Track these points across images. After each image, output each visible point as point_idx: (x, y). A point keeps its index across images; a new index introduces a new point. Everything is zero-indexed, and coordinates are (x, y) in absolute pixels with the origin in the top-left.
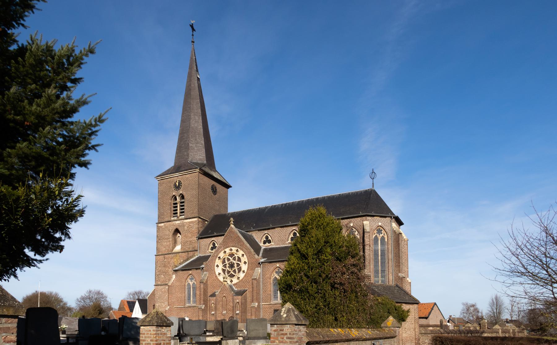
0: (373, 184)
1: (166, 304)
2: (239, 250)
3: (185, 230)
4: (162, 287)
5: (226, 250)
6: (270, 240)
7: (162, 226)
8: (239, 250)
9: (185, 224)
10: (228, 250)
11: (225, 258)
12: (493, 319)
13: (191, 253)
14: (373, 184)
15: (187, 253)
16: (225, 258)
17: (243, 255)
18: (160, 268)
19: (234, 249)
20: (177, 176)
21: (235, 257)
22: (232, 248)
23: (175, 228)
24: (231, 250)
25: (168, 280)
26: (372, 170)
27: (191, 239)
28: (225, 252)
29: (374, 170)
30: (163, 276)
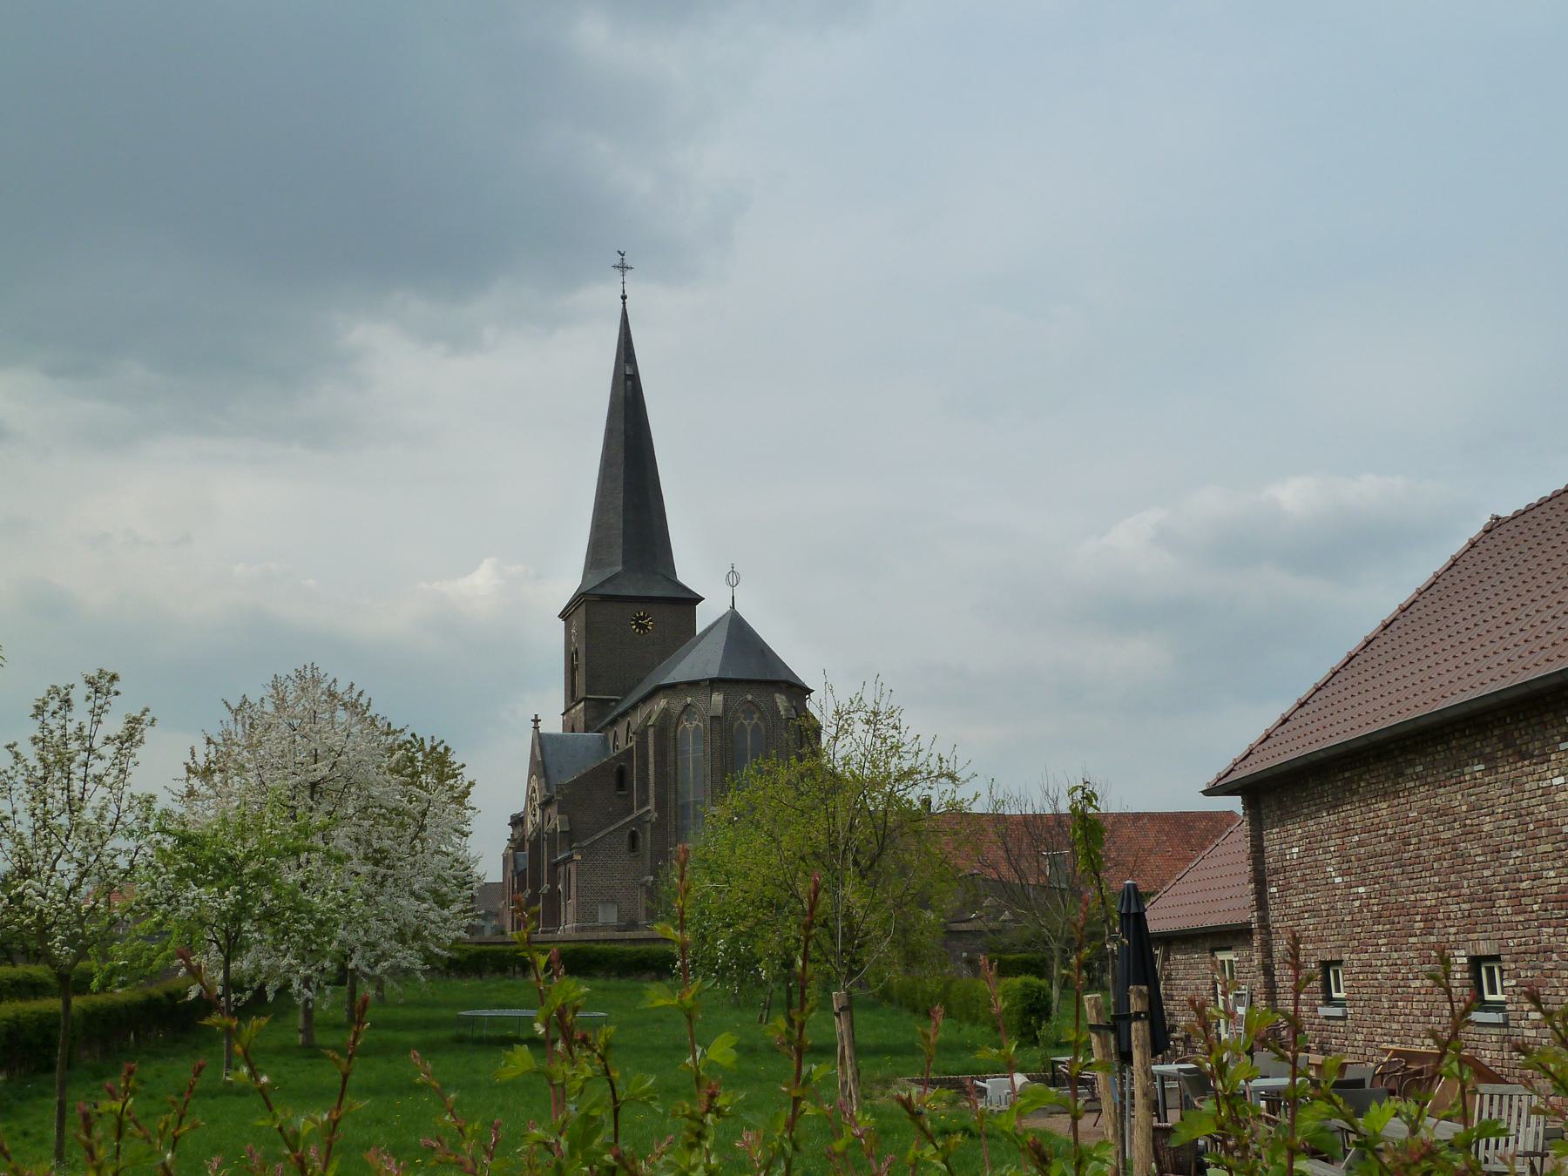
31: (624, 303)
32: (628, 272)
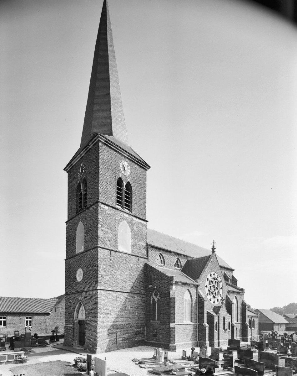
6: (178, 265)
9: (134, 222)
15: (137, 258)
28: (211, 275)
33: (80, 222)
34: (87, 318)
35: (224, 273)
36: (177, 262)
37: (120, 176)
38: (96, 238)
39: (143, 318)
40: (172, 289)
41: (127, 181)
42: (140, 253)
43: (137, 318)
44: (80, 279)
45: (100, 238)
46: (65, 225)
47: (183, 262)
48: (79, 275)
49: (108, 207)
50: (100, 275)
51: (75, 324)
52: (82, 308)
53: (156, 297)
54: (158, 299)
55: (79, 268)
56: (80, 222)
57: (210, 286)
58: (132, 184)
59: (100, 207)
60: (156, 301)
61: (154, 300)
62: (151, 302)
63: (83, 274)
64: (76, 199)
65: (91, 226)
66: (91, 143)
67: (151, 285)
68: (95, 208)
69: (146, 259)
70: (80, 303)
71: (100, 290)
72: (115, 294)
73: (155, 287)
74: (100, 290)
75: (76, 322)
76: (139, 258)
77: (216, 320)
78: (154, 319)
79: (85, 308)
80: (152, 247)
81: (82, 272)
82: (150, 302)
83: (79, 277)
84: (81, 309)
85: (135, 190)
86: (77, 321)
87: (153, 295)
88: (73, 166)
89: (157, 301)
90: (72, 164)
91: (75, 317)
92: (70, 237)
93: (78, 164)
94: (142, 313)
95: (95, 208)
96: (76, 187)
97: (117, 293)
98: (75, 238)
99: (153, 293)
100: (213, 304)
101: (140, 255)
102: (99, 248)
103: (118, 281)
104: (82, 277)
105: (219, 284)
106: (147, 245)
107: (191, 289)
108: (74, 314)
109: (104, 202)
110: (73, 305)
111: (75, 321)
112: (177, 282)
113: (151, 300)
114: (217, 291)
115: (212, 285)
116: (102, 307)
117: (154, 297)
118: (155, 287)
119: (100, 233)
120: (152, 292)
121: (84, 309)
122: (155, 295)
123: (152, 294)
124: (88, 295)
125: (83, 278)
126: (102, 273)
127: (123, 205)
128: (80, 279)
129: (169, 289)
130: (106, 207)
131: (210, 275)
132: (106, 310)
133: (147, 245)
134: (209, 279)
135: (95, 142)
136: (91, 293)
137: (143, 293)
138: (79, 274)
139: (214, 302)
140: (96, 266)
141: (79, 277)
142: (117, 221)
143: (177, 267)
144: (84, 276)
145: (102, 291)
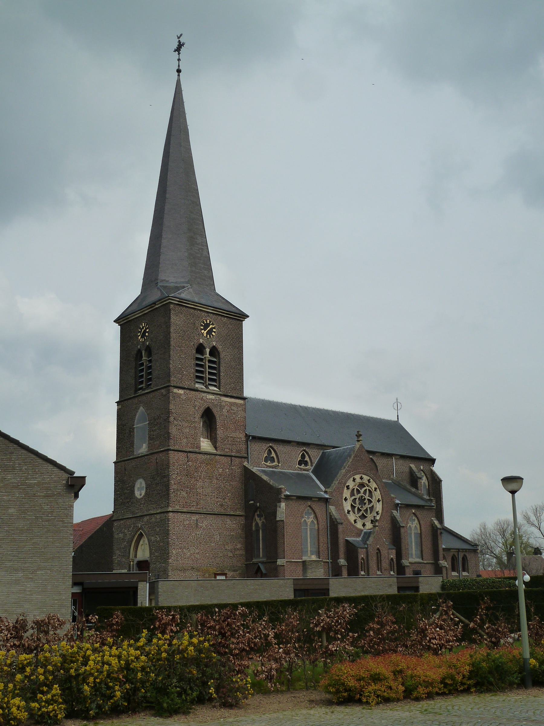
0: (398, 416)
1: (191, 552)
2: (371, 480)
3: (222, 415)
4: (184, 516)
5: (356, 477)
6: (306, 461)
7: (181, 394)
8: (371, 480)
9: (223, 404)
10: (357, 477)
11: (354, 489)
12: (417, 635)
13: (237, 459)
14: (398, 416)
15: (229, 459)
16: (354, 489)
17: (376, 489)
18: (179, 478)
19: (366, 478)
20: (208, 312)
21: (357, 489)
22: (364, 476)
23: (206, 406)
24: (361, 478)
25: (194, 504)
26: (396, 399)
27: (233, 435)
28: (354, 480)
29: (398, 399)
30: (184, 494)
31: (179, 75)
32: (183, 49)
33: (141, 408)
34: (152, 556)
35: (410, 468)
36: (303, 456)
37: (201, 341)
38: (167, 436)
39: (241, 555)
40: (280, 507)
41: (211, 346)
42: (234, 451)
43: (232, 555)
44: (141, 495)
45: (171, 437)
46: (115, 407)
47: (315, 455)
48: (138, 488)
49: (183, 391)
50: (172, 491)
51: (131, 567)
52: (144, 541)
53: (260, 520)
54: (263, 522)
55: (140, 478)
56: (141, 408)
57: (353, 497)
58: (220, 348)
59: (172, 392)
60: (260, 525)
61: (257, 524)
62: (254, 528)
63: (146, 488)
64: (133, 371)
65: (158, 417)
66: (158, 303)
67: (252, 500)
68: (164, 393)
69: (245, 458)
70: (141, 534)
71: (172, 512)
72: (194, 517)
73: (258, 504)
74: (172, 512)
75: (133, 565)
76: (233, 458)
77: (362, 555)
78: (258, 556)
79: (148, 540)
80: (254, 438)
81: (144, 485)
82: (252, 529)
83: (140, 491)
84: (141, 542)
85: (225, 355)
86: (135, 562)
87: (256, 516)
88: (129, 321)
89: (262, 525)
90: (128, 318)
91: (131, 557)
92: (124, 426)
93: (138, 320)
94: (239, 546)
95: (164, 393)
96: (134, 352)
97: (197, 516)
98: (131, 430)
99: (256, 514)
100: (362, 528)
101: (233, 454)
102: (170, 452)
103: (198, 497)
104: (143, 492)
105: (373, 494)
106: (247, 436)
107: (314, 506)
108: (130, 550)
109: (178, 385)
110: (128, 537)
111: (132, 563)
112: (287, 497)
113: (254, 524)
114: (367, 506)
115: (358, 496)
116: (175, 537)
117: (258, 519)
118: (258, 504)
119: (173, 430)
120: (256, 511)
121: (146, 542)
122: (258, 516)
123: (254, 515)
124: (153, 520)
125: (146, 493)
126: (175, 487)
127: (206, 382)
128: (141, 495)
129: (276, 506)
130: (181, 392)
131: (352, 479)
132: (181, 542)
133: (247, 436)
134: (351, 487)
135: (165, 303)
136: (158, 516)
137: (241, 514)
138: (139, 486)
139: (364, 525)
140: (167, 477)
141: (140, 491)
142: (197, 408)
143: (303, 465)
144: (148, 491)
145: (175, 514)
